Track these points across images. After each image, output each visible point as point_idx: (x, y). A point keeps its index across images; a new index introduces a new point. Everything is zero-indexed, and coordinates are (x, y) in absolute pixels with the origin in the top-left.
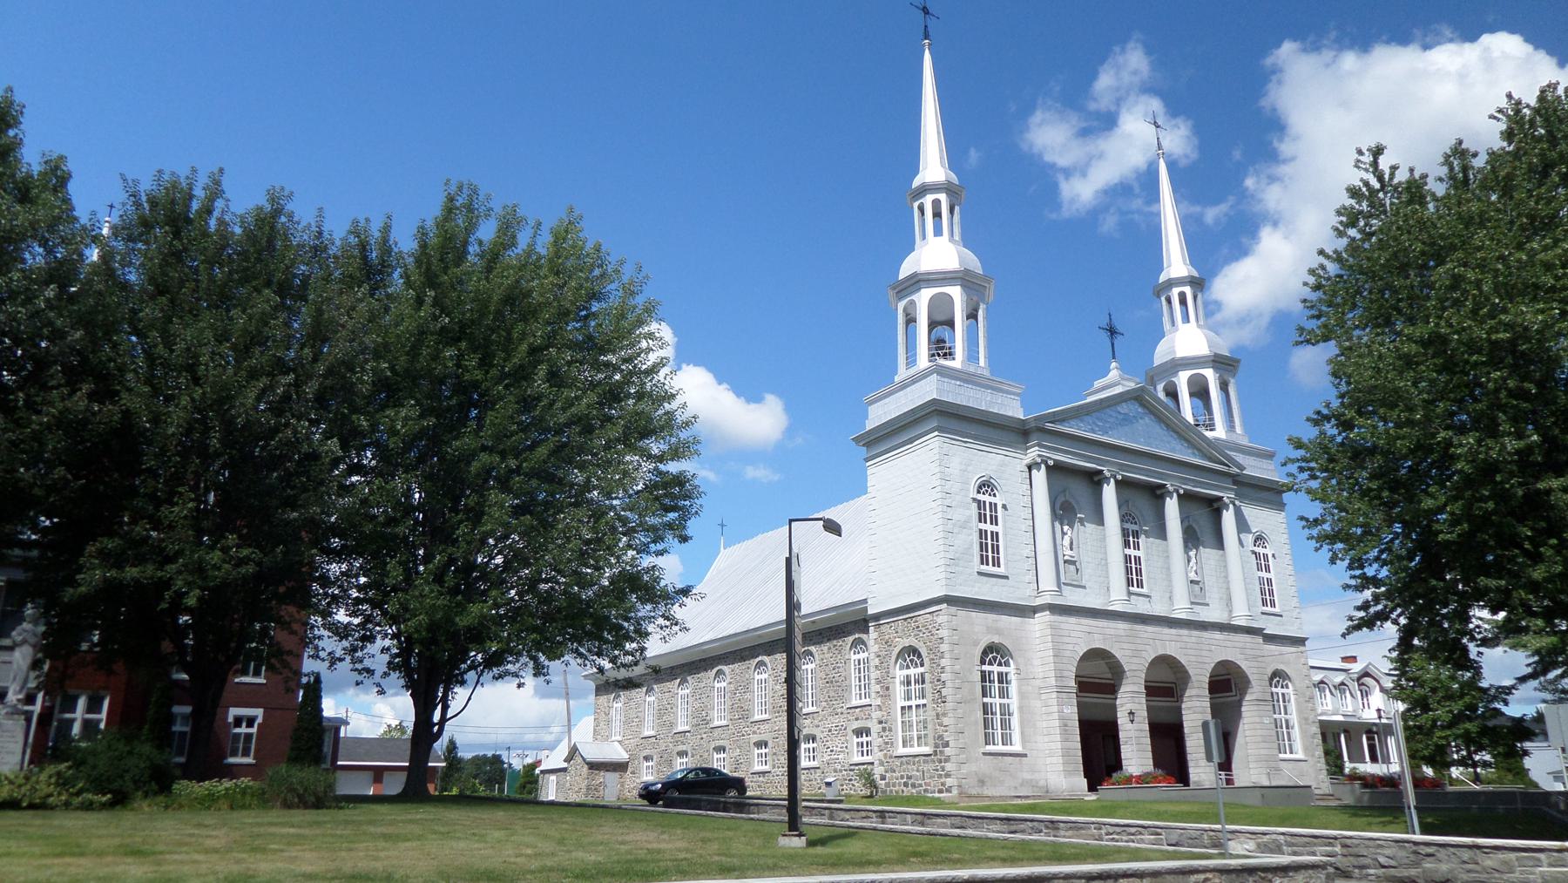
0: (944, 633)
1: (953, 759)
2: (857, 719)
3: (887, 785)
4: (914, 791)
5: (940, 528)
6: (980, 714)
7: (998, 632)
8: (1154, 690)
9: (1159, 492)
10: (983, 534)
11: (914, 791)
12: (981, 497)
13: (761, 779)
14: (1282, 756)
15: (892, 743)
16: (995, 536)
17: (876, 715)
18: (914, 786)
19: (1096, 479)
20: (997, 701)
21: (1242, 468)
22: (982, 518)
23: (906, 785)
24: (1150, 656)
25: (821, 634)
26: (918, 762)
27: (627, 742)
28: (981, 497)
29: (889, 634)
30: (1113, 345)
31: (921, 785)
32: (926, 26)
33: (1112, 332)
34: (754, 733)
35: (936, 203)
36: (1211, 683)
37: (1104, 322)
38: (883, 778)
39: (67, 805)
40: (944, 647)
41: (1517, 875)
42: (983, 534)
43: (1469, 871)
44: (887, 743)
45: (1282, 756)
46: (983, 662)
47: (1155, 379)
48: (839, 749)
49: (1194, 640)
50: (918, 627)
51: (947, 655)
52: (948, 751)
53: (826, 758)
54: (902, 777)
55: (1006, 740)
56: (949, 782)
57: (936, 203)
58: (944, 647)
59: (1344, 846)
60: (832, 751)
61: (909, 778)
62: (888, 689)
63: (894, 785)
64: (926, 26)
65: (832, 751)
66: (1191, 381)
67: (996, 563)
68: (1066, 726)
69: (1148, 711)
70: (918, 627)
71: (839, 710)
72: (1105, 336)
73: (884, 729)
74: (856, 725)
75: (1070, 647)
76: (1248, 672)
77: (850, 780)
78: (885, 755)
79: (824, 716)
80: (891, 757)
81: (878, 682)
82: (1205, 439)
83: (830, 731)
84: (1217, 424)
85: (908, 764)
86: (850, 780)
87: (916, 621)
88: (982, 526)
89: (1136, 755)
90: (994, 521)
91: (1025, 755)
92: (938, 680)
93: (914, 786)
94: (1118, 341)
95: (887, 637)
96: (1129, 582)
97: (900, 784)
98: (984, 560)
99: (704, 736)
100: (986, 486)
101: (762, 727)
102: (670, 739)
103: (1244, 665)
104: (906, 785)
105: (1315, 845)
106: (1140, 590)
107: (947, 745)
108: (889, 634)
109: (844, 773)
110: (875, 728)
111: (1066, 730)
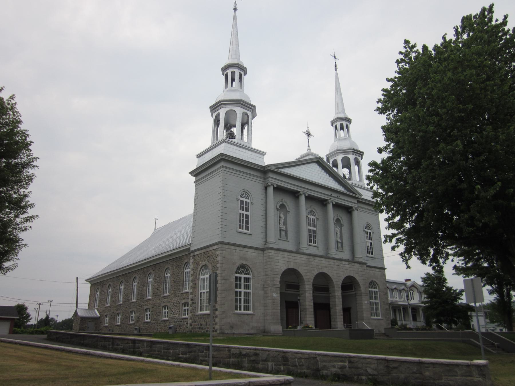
0: (219, 259)
1: (219, 316)
2: (184, 299)
3: (193, 328)
4: (203, 331)
5: (221, 211)
6: (233, 297)
7: (245, 259)
8: (316, 288)
9: (325, 203)
10: (241, 215)
12: (242, 199)
13: (147, 325)
14: (373, 317)
15: (196, 309)
16: (247, 217)
17: (190, 296)
18: (202, 329)
19: (297, 195)
20: (243, 290)
21: (361, 195)
22: (242, 208)
23: (199, 328)
24: (316, 272)
26: (205, 318)
27: (100, 309)
28: (242, 199)
30: (308, 140)
31: (205, 329)
32: (235, 2)
33: (308, 134)
34: (146, 305)
35: (233, 73)
36: (342, 286)
37: (305, 130)
38: (191, 325)
40: (218, 265)
41: (443, 381)
42: (241, 215)
43: (416, 378)
45: (373, 317)
46: (237, 273)
47: (329, 159)
48: (176, 312)
49: (327, 263)
50: (209, 256)
51: (219, 269)
52: (217, 313)
53: (172, 316)
54: (198, 325)
55: (247, 308)
56: (217, 327)
57: (233, 73)
58: (218, 265)
59: (350, 362)
60: (174, 313)
61: (201, 325)
62: (195, 284)
63: (195, 328)
64: (235, 2)
65: (174, 313)
66: (343, 159)
67: (247, 228)
68: (274, 302)
69: (313, 297)
70: (209, 256)
71: (178, 295)
72: (306, 136)
73: (193, 303)
75: (279, 267)
76: (359, 281)
77: (180, 326)
78: (193, 315)
80: (195, 316)
82: (348, 184)
83: (174, 304)
85: (201, 319)
86: (180, 326)
87: (208, 254)
88: (242, 212)
89: (309, 319)
90: (247, 210)
91: (254, 315)
93: (202, 329)
94: (311, 138)
95: (197, 261)
96: (310, 241)
98: (241, 227)
99: (127, 306)
100: (245, 194)
102: (115, 308)
103: (358, 278)
104: (199, 328)
105: (335, 361)
106: (314, 244)
107: (216, 310)
108: (198, 259)
109: (178, 323)
110: (190, 302)
111: (274, 304)
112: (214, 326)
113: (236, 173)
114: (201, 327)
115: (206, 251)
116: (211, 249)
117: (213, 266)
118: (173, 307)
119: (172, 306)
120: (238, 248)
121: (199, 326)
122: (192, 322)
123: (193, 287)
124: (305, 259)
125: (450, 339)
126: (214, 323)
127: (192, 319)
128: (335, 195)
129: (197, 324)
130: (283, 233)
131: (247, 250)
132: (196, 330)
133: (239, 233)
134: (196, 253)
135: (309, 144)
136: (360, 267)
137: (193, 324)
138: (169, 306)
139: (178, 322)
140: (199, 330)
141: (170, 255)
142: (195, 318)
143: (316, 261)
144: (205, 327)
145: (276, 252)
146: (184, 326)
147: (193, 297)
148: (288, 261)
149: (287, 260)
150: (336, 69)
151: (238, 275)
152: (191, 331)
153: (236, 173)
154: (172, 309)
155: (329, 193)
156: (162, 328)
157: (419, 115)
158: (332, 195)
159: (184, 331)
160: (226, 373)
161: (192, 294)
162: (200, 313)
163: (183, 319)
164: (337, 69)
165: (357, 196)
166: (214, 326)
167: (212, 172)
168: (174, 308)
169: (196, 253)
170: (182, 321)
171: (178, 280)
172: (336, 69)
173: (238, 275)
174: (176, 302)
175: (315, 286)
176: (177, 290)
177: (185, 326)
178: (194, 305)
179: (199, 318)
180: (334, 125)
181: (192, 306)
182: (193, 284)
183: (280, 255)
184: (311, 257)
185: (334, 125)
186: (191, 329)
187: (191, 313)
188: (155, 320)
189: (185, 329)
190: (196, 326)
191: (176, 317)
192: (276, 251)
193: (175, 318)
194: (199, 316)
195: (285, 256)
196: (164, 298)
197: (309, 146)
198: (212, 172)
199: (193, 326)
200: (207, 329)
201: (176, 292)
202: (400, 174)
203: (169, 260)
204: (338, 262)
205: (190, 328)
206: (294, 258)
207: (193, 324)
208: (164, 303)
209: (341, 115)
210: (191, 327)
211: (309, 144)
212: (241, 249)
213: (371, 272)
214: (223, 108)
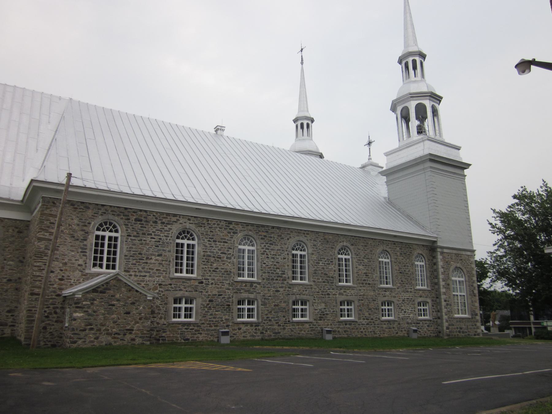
2: (421, 296)
3: (450, 332)
4: (463, 335)
11: (463, 335)
18: (463, 332)
23: (459, 332)
25: (394, 244)
29: (448, 258)
34: (340, 294)
35: (414, 62)
38: (448, 328)
39: (103, 285)
44: (449, 311)
54: (457, 328)
57: (414, 62)
60: (405, 312)
61: (461, 328)
64: (302, 56)
65: (405, 312)
71: (409, 290)
73: (447, 305)
74: (420, 300)
78: (449, 317)
79: (399, 292)
80: (452, 318)
81: (444, 281)
83: (403, 301)
84: (342, 256)
92: (472, 286)
93: (463, 332)
97: (456, 332)
101: (348, 291)
104: (459, 332)
108: (448, 258)
112: (476, 330)
114: (461, 331)
115: (457, 253)
116: (464, 253)
117: (468, 272)
118: (403, 305)
119: (400, 302)
121: (459, 329)
122: (449, 325)
123: (445, 286)
126: (475, 327)
127: (449, 322)
129: (456, 327)
132: (455, 334)
134: (445, 251)
135: (370, 153)
137: (450, 327)
138: (396, 302)
139: (414, 323)
140: (459, 334)
141: (395, 236)
142: (452, 321)
144: (466, 330)
146: (424, 329)
147: (447, 298)
150: (302, 63)
151: (180, 241)
152: (448, 335)
154: (402, 306)
156: (385, 331)
159: (424, 335)
161: (446, 295)
162: (456, 316)
163: (421, 320)
164: (303, 63)
166: (476, 330)
167: (455, 173)
168: (404, 306)
169: (445, 251)
170: (421, 323)
171: (407, 272)
172: (302, 63)
173: (180, 241)
174: (407, 299)
176: (407, 284)
177: (425, 329)
178: (449, 307)
179: (457, 321)
181: (446, 308)
182: (445, 284)
186: (448, 333)
187: (446, 315)
188: (367, 319)
189: (426, 332)
190: (455, 329)
191: (409, 317)
193: (408, 319)
194: (458, 320)
196: (384, 290)
197: (370, 156)
198: (455, 173)
199: (450, 330)
200: (468, 333)
201: (405, 286)
203: (386, 240)
205: (447, 331)
207: (450, 327)
208: (385, 296)
209: (302, 114)
210: (448, 330)
211: (370, 153)
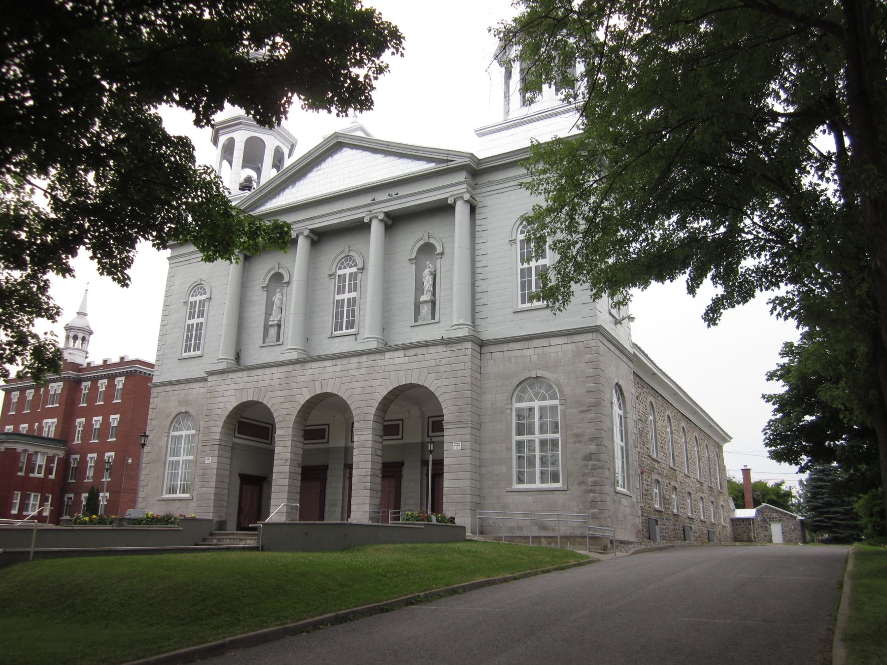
7: (187, 403)
75: (222, 405)
111: (204, 478)
113: (187, 258)
120: (177, 387)
124: (282, 375)
125: (313, 522)
128: (382, 196)
130: (273, 332)
131: (191, 385)
133: (183, 361)
136: (447, 354)
143: (309, 372)
145: (220, 377)
148: (242, 389)
149: (241, 386)
153: (187, 258)
155: (366, 200)
157: (39, 228)
158: (377, 200)
160: (256, 645)
165: (459, 161)
175: (271, 429)
180: (223, 139)
183: (227, 382)
184: (298, 366)
185: (223, 139)
192: (220, 376)
195: (238, 380)
202: (209, 211)
204: (372, 357)
206: (255, 379)
212: (182, 386)
213: (529, 352)
214: (243, 131)
